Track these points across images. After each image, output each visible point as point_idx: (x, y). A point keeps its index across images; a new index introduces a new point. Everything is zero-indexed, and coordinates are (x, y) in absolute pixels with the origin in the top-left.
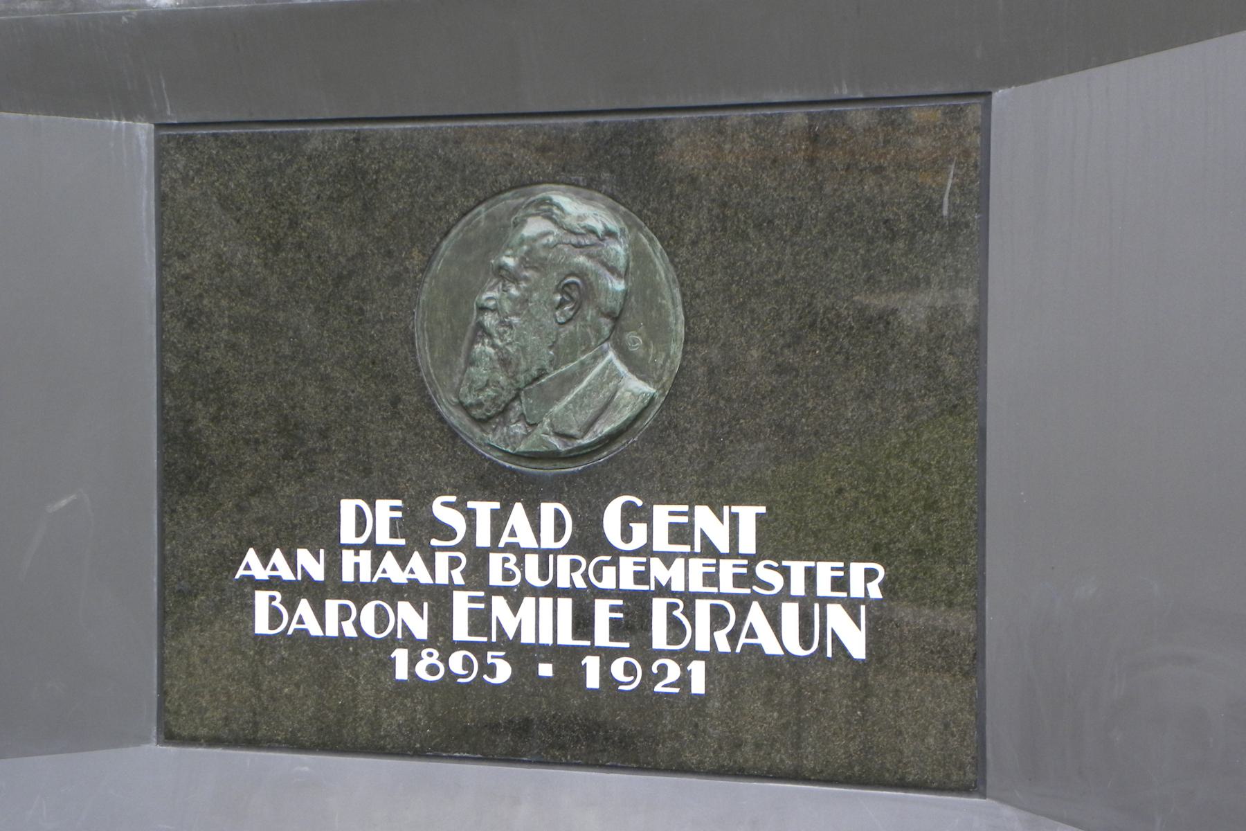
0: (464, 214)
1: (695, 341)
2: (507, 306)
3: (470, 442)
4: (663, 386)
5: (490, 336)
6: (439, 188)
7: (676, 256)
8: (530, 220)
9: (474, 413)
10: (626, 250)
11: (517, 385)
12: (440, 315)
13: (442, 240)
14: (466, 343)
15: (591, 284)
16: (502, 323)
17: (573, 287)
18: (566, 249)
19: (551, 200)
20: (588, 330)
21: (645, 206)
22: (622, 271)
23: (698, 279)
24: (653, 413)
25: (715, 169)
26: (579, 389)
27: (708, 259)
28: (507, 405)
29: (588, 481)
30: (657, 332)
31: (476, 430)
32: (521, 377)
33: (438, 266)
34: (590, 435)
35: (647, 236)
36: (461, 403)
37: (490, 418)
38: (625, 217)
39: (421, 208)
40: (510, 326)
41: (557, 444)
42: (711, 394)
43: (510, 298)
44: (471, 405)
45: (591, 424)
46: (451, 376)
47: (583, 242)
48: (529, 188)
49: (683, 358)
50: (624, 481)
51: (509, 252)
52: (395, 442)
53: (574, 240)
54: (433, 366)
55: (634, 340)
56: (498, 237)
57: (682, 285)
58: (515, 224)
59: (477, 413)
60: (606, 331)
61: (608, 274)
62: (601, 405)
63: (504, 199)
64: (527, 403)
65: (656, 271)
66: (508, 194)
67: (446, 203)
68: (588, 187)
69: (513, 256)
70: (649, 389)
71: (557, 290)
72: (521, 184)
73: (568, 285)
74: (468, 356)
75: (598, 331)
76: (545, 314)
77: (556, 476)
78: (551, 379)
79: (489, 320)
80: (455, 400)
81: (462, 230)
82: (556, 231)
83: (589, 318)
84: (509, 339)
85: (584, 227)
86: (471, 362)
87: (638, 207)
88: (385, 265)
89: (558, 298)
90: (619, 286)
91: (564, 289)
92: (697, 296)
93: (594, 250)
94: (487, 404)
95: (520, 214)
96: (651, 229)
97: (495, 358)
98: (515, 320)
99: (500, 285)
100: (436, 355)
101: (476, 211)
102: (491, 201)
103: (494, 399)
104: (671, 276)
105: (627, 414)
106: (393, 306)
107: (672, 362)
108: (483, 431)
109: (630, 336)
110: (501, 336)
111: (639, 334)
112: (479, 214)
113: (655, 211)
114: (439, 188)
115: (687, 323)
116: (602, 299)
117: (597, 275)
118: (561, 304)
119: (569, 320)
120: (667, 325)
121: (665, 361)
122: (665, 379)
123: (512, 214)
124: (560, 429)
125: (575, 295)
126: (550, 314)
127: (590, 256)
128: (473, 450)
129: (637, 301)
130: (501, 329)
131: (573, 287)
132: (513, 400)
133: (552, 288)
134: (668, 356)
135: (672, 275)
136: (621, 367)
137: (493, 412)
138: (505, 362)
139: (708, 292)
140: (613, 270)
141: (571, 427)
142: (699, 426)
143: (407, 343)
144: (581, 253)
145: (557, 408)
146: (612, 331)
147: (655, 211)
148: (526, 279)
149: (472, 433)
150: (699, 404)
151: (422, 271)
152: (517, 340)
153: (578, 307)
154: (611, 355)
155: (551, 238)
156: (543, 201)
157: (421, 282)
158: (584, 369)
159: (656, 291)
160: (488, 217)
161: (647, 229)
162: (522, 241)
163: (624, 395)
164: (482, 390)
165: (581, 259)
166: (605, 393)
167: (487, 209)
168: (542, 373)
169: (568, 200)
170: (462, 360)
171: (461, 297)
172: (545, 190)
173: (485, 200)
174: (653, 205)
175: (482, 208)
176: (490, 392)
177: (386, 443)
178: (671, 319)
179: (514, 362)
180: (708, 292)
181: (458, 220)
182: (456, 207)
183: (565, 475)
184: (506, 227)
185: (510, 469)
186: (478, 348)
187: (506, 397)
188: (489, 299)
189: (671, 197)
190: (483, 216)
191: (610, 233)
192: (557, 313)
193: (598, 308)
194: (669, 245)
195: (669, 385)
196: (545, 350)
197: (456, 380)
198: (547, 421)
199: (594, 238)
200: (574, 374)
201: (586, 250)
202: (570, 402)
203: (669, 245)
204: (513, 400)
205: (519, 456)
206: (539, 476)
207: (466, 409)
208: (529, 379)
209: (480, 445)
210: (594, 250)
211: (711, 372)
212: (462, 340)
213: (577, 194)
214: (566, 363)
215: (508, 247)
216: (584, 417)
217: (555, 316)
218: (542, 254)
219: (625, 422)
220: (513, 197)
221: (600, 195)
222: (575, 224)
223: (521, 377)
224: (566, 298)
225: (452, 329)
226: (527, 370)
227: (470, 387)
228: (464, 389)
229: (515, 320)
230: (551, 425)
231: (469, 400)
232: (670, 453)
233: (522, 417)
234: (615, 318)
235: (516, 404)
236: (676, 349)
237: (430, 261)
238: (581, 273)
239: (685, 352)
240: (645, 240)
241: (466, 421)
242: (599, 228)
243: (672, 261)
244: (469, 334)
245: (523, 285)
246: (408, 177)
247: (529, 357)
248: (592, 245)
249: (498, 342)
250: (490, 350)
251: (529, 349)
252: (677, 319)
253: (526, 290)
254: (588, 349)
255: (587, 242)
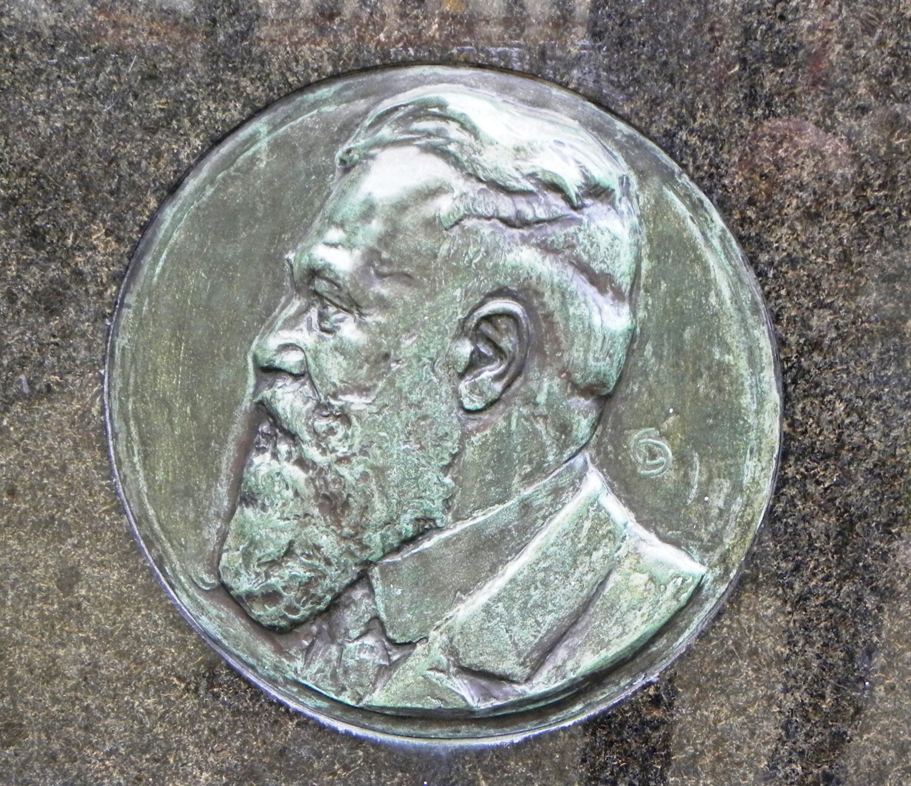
0: (217, 142)
1: (808, 452)
2: (335, 369)
3: (249, 675)
4: (724, 559)
5: (292, 436)
6: (152, 77)
7: (763, 246)
8: (386, 156)
9: (257, 611)
10: (634, 231)
11: (365, 555)
12: (166, 383)
13: (162, 203)
14: (230, 451)
15: (548, 316)
16: (322, 408)
17: (503, 323)
18: (485, 229)
19: (442, 106)
20: (540, 426)
21: (682, 123)
22: (625, 282)
23: (821, 305)
24: (697, 621)
25: (869, 30)
26: (514, 568)
27: (845, 258)
28: (337, 596)
29: (536, 768)
30: (711, 429)
31: (265, 649)
32: (374, 538)
33: (154, 268)
34: (546, 671)
35: (686, 196)
36: (224, 588)
37: (296, 624)
38: (627, 148)
39: (108, 127)
40: (344, 417)
41: (465, 693)
42: (842, 579)
43: (340, 349)
44: (250, 596)
45: (547, 650)
46: (197, 526)
47: (529, 213)
48: (379, 77)
49: (777, 494)
50: (624, 770)
51: (334, 234)
52: (72, 671)
53: (506, 206)
54: (153, 500)
55: (652, 448)
56: (304, 191)
57: (776, 319)
58: (347, 167)
59: (266, 613)
60: (582, 426)
61: (592, 290)
62: (574, 603)
63: (315, 105)
64: (388, 596)
65: (708, 284)
66: (324, 92)
67: (171, 115)
68: (532, 75)
69: (349, 245)
70: (689, 566)
71: (463, 331)
72: (363, 66)
73: (488, 318)
74: (238, 480)
75: (565, 428)
76: (432, 391)
77: (460, 754)
78: (447, 543)
79: (288, 399)
80: (210, 580)
81: (211, 180)
82: (460, 184)
83: (541, 398)
84: (342, 450)
85: (532, 175)
86: (244, 495)
87: (663, 123)
88: (28, 264)
89: (465, 349)
90: (612, 319)
91: (482, 329)
92: (816, 345)
93: (557, 233)
94: (289, 596)
95: (358, 142)
96: (699, 181)
97: (309, 491)
98: (356, 402)
99: (314, 313)
100: (160, 476)
101: (244, 134)
102: (282, 110)
103: (306, 586)
104: (745, 296)
105: (638, 627)
106: (50, 360)
107: (748, 504)
108: (280, 651)
109: (641, 439)
110: (320, 438)
111: (665, 435)
112: (253, 139)
113: (711, 136)
114: (152, 77)
115: (786, 413)
116: (577, 354)
117: (565, 296)
118: (475, 363)
119: (491, 404)
120: (736, 415)
121: (728, 502)
122: (728, 541)
123: (336, 142)
124: (471, 659)
125: (507, 342)
126: (445, 388)
127: (547, 248)
128: (257, 693)
129: (658, 355)
130: (321, 424)
131: (503, 323)
132: (352, 585)
133: (452, 327)
134: (738, 488)
135: (752, 290)
136: (618, 511)
137: (304, 612)
138: (333, 504)
139: (842, 338)
140: (601, 281)
141: (501, 655)
142: (810, 652)
143: (90, 447)
144: (525, 240)
145: (466, 610)
146: (594, 428)
147: (711, 136)
148: (383, 304)
149: (253, 654)
150: (814, 602)
151: (117, 278)
152: (364, 452)
153: (516, 372)
154: (594, 482)
155: (444, 206)
156: (421, 110)
157: (118, 305)
158: (529, 518)
159: (711, 329)
160: (276, 146)
161: (685, 179)
162: (369, 211)
163: (628, 584)
164: (275, 563)
165: (525, 258)
166: (584, 576)
167: (275, 127)
168: (425, 527)
169: (486, 106)
170: (222, 489)
171: (214, 338)
172: (418, 82)
173: (268, 105)
174: (704, 120)
175: (260, 125)
176: (296, 569)
177: (51, 674)
178: (747, 400)
179: (356, 502)
180: (842, 338)
181: (202, 156)
182: (195, 123)
183: (480, 753)
184: (322, 173)
185: (348, 734)
186: (262, 463)
187: (335, 579)
188: (286, 347)
189: (751, 99)
190: (263, 144)
191: (596, 191)
192: (463, 386)
193: (566, 373)
194: (744, 220)
195: (738, 557)
196: (431, 476)
197: (211, 533)
198: (437, 638)
199: (558, 205)
200: (504, 531)
201: (538, 235)
202: (498, 599)
203: (744, 220)
204: (352, 585)
205: (370, 714)
206: (419, 752)
207: (240, 603)
208: (393, 541)
209: (273, 681)
210: (557, 233)
211: (847, 528)
212: (223, 443)
213: (504, 90)
214: (485, 504)
215: (331, 222)
216: (528, 636)
217: (456, 393)
218: (425, 242)
219: (632, 646)
220: (338, 97)
221: (564, 94)
222: (508, 170)
223: (374, 538)
224: (485, 349)
225: (194, 416)
226: (390, 522)
227: (247, 556)
228: (230, 558)
229: (356, 402)
230: (451, 651)
231: (244, 584)
232: (740, 711)
233: (375, 625)
234: (602, 395)
235: (358, 593)
236: (759, 472)
237: (135, 256)
238: (526, 291)
239: (781, 482)
240: (680, 207)
241: (239, 627)
242: (572, 181)
243: (752, 260)
244: (237, 430)
245: (375, 318)
246: (74, 51)
247: (393, 493)
248: (551, 221)
249: (313, 453)
250: (298, 474)
251: (394, 475)
252: (761, 400)
253: (383, 329)
254: (539, 470)
255: (542, 214)
